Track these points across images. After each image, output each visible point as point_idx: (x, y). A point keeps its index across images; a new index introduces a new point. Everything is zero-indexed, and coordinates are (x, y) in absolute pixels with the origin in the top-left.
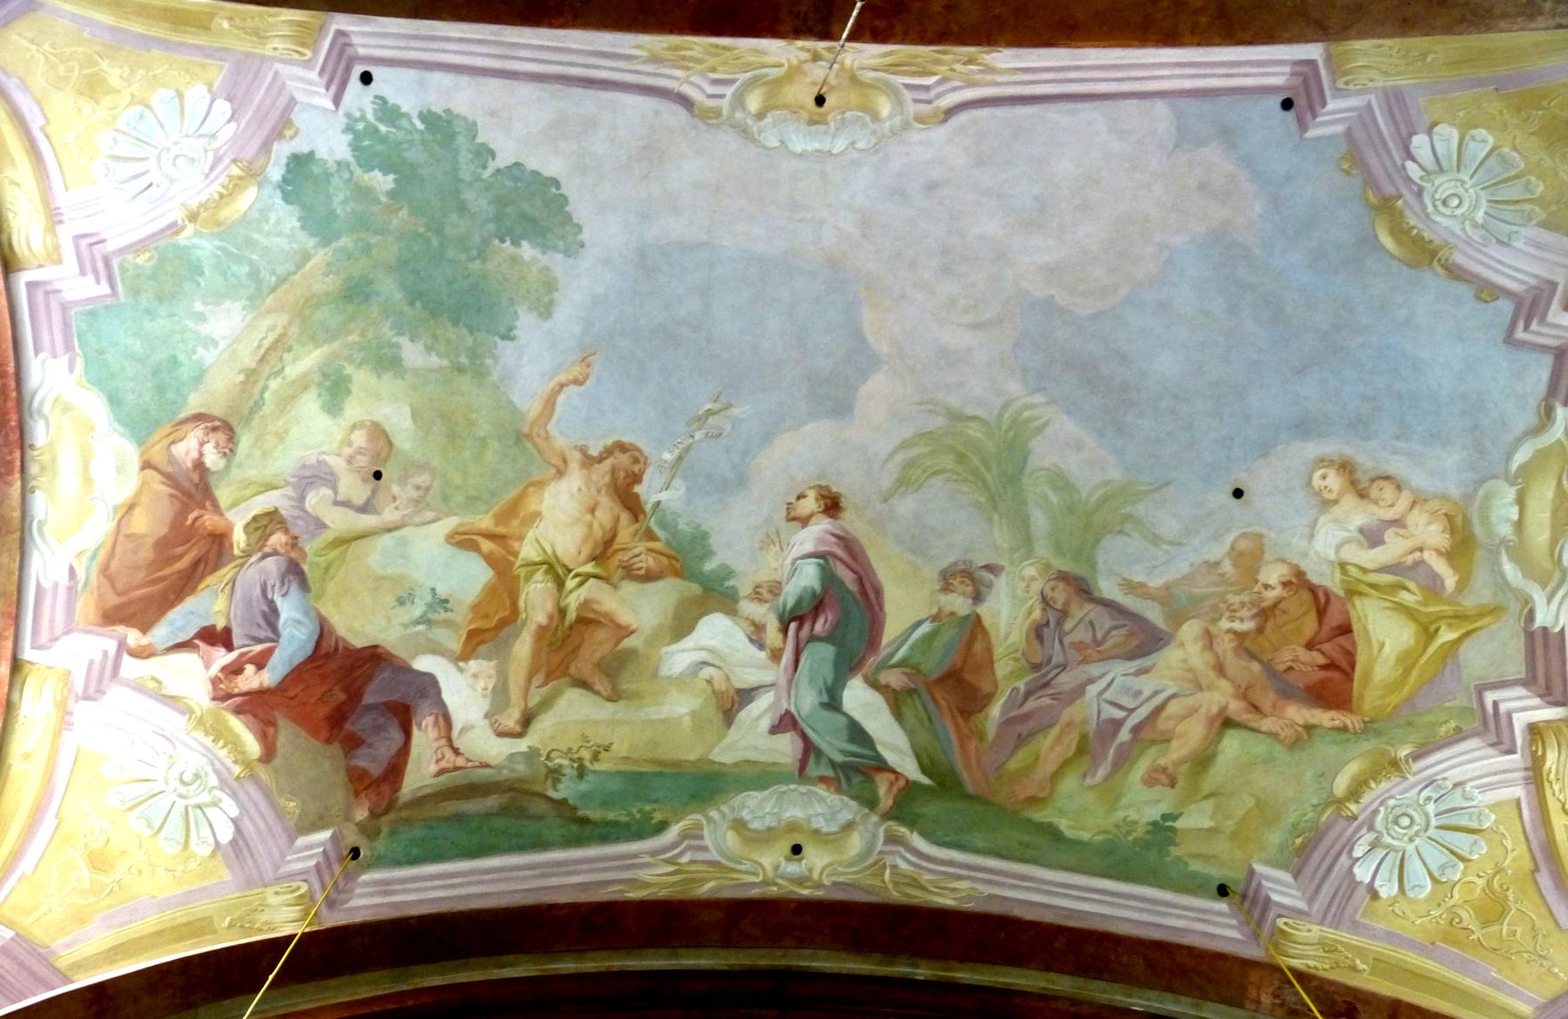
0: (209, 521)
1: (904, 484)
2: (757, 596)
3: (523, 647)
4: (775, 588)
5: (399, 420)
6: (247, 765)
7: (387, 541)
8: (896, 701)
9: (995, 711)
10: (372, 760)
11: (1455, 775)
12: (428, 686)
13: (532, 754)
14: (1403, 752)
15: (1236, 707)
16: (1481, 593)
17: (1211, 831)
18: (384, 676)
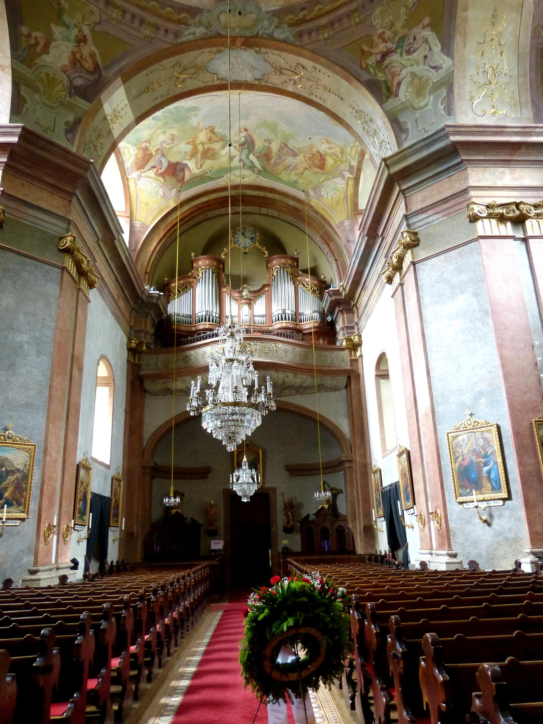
0: (149, 152)
1: (258, 128)
2: (235, 142)
3: (199, 155)
4: (238, 141)
5: (174, 132)
6: (162, 183)
7: (176, 147)
8: (258, 158)
9: (272, 161)
10: (180, 177)
11: (337, 182)
12: (186, 165)
13: (203, 170)
14: (331, 177)
15: (308, 167)
16: (344, 158)
17: (303, 183)
18: (179, 166)
